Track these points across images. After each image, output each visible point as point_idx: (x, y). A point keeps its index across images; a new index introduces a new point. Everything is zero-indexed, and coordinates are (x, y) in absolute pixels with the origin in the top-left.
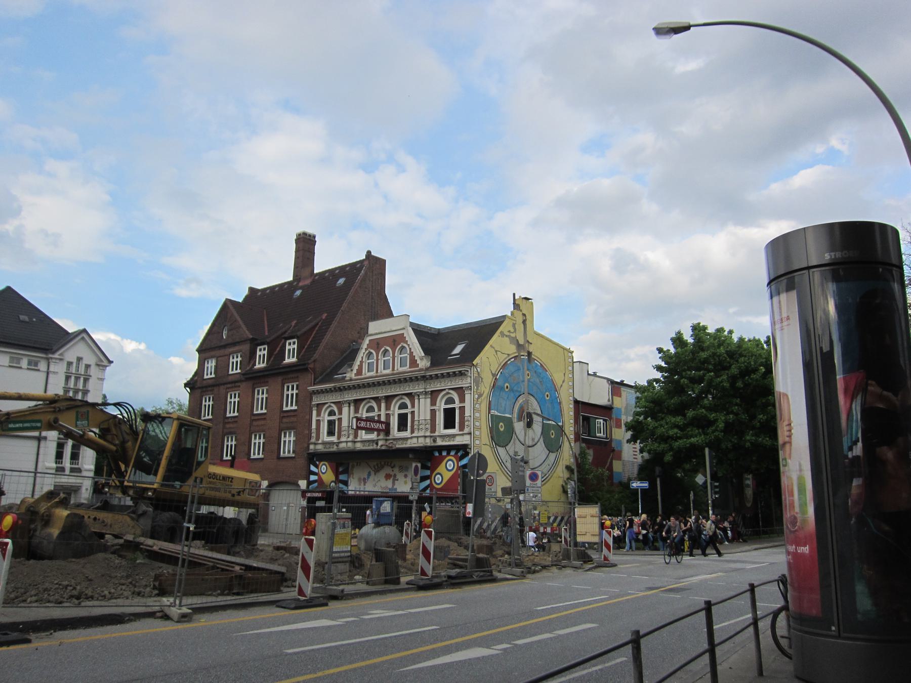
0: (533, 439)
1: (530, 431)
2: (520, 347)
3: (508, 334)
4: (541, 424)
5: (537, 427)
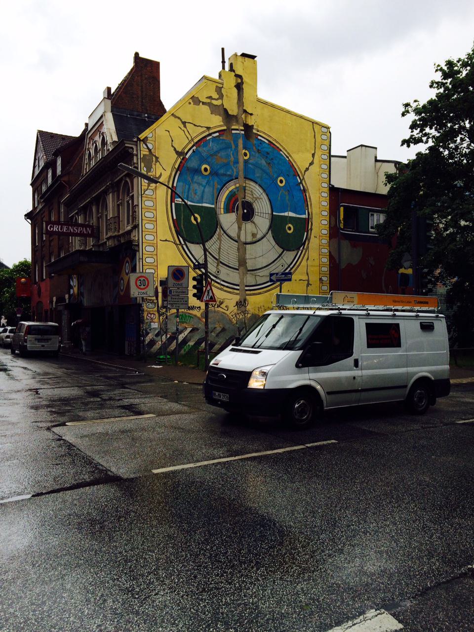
0: (254, 235)
1: (248, 227)
2: (228, 117)
3: (208, 101)
4: (268, 216)
5: (262, 222)
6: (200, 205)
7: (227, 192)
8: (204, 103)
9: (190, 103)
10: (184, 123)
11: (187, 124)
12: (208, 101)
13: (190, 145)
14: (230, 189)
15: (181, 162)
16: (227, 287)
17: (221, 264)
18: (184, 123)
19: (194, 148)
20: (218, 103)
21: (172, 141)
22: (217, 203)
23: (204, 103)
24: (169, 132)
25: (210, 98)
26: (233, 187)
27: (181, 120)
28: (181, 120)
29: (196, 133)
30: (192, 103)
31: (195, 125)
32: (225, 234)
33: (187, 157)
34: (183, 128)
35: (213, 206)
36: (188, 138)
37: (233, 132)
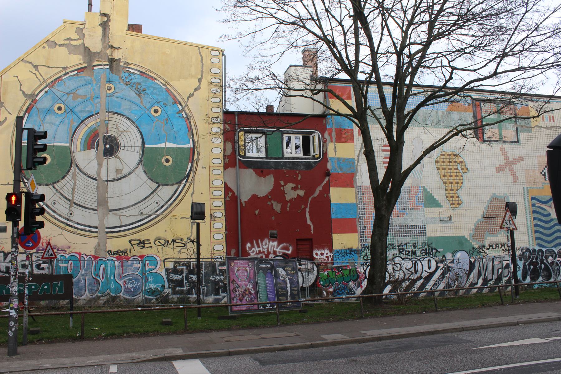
3: (67, 42)
6: (52, 144)
7: (86, 128)
8: (60, 45)
9: (44, 47)
10: (36, 67)
11: (39, 67)
12: (67, 42)
13: (42, 87)
14: (89, 125)
15: (30, 104)
16: (82, 230)
17: (74, 206)
18: (36, 67)
19: (47, 89)
20: (80, 42)
21: (21, 85)
22: (72, 140)
23: (60, 45)
24: (17, 77)
25: (69, 39)
26: (94, 122)
27: (33, 65)
28: (33, 65)
29: (49, 74)
30: (47, 47)
31: (49, 67)
32: (80, 173)
33: (38, 98)
34: (34, 71)
35: (68, 145)
36: (39, 80)
37: (95, 68)
